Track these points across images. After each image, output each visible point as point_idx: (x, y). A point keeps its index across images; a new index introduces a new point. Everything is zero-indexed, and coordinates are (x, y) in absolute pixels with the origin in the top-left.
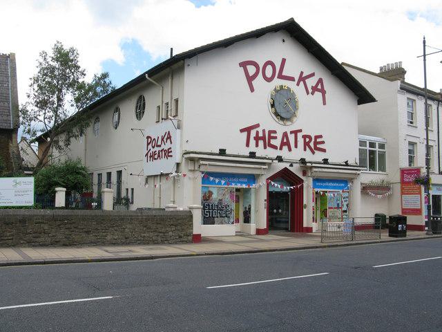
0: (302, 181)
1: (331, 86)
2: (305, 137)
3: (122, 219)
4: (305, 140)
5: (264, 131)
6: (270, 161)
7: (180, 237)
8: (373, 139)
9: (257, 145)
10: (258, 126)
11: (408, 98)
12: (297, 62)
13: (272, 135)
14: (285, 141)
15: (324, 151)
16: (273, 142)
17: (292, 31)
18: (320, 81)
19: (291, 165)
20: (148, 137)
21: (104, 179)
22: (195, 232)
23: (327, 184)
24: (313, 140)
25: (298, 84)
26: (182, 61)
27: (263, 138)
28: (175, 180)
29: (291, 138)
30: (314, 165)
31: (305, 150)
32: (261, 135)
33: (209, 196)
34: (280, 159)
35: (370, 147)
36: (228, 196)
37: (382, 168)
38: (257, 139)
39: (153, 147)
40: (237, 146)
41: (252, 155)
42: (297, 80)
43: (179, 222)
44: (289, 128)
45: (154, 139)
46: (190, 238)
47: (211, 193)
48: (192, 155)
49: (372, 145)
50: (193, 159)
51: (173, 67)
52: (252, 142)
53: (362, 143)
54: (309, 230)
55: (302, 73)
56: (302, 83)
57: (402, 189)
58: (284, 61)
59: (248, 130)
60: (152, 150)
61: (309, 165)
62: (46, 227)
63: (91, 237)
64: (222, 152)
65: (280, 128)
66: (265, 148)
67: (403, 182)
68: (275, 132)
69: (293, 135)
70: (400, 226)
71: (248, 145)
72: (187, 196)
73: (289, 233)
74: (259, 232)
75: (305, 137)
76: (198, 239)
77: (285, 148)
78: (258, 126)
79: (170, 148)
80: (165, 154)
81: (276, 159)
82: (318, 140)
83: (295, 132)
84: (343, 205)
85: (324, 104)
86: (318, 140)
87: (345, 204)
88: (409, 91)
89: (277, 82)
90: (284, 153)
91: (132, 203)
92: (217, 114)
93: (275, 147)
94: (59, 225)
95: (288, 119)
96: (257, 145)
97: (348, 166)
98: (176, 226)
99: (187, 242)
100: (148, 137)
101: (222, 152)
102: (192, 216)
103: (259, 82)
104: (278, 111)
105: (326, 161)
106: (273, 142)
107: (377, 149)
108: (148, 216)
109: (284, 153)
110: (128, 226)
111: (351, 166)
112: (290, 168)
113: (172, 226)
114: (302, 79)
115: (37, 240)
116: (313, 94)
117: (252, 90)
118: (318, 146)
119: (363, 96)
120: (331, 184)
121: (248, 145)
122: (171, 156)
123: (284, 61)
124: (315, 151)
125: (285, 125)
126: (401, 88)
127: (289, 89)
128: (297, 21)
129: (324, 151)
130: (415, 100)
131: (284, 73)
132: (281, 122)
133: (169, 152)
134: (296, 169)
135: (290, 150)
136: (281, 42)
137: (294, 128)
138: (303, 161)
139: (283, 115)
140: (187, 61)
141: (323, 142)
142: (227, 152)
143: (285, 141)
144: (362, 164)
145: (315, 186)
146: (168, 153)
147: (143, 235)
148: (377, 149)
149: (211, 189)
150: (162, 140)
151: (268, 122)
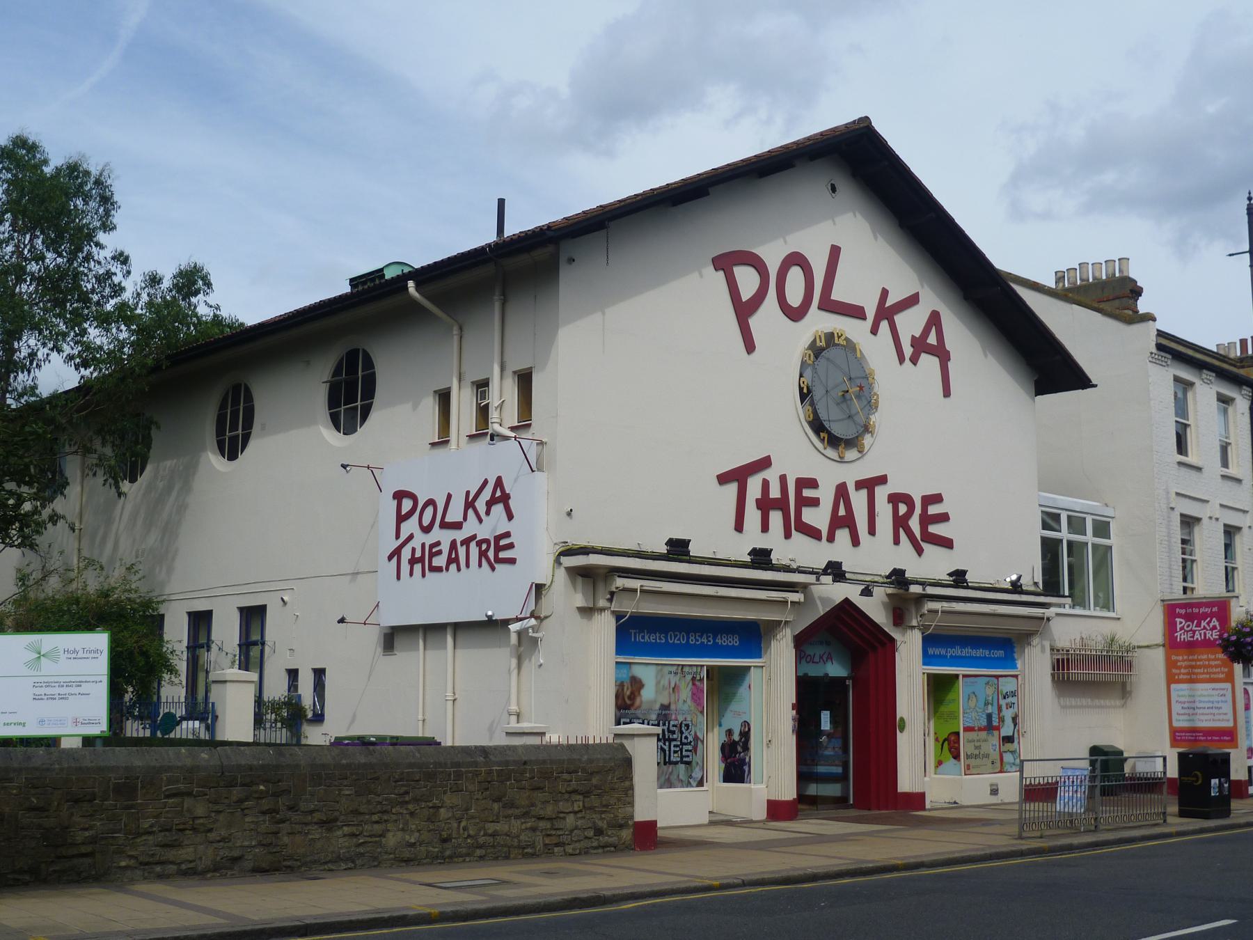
0: (892, 640)
1: (960, 335)
2: (895, 499)
3: (430, 776)
4: (895, 510)
5: (783, 479)
6: (811, 579)
7: (599, 832)
8: (1078, 503)
9: (765, 528)
10: (765, 463)
11: (1177, 379)
12: (873, 264)
13: (807, 493)
14: (842, 512)
15: (947, 543)
16: (809, 516)
17: (859, 160)
18: (935, 320)
19: (867, 592)
20: (399, 496)
21: (226, 631)
22: (641, 813)
23: (957, 651)
24: (918, 510)
25: (874, 330)
26: (550, 248)
27: (782, 504)
28: (528, 643)
29: (859, 500)
30: (931, 590)
31: (897, 541)
32: (775, 493)
33: (633, 696)
34: (835, 571)
35: (1096, 533)
36: (686, 692)
37: (1106, 602)
38: (765, 505)
39: (426, 530)
40: (718, 537)
41: (761, 558)
42: (871, 313)
43: (594, 781)
44: (851, 474)
45: (431, 502)
46: (626, 834)
47: (637, 684)
48: (594, 560)
49: (1076, 524)
50: (592, 574)
51: (516, 271)
52: (753, 515)
53: (1050, 520)
54: (917, 800)
55: (885, 293)
56: (884, 325)
57: (1170, 665)
58: (835, 252)
59: (738, 476)
60: (420, 538)
61: (915, 589)
62: (200, 810)
63: (340, 841)
64: (678, 549)
65: (830, 472)
66: (788, 535)
67: (1172, 644)
68: (813, 484)
69: (864, 492)
70: (1215, 782)
71: (739, 527)
72: (567, 693)
73: (853, 813)
74: (777, 810)
75: (895, 499)
76: (647, 836)
77: (843, 535)
78: (765, 463)
79: (507, 535)
80: (483, 554)
81: (825, 572)
82: (933, 510)
83: (869, 485)
84: (1002, 720)
85: (947, 393)
86: (933, 510)
87: (1008, 714)
88: (1179, 357)
89: (819, 322)
90: (840, 550)
91: (319, 718)
92: (654, 417)
93: (814, 533)
94: (241, 801)
95: (851, 443)
96: (765, 528)
97: (1023, 592)
98: (586, 794)
99: (617, 849)
100: (399, 496)
101: (678, 549)
102: (628, 762)
103: (767, 318)
104: (823, 415)
105: (959, 578)
106: (809, 516)
107: (1089, 538)
108: (507, 763)
109: (840, 550)
110: (449, 799)
111: (787, 569)
112: (862, 603)
113: (565, 794)
114: (886, 313)
115: (171, 854)
116: (914, 360)
117: (750, 347)
118: (933, 529)
119: (1050, 368)
120: (968, 652)
121: (739, 527)
122: (512, 561)
123: (835, 252)
124: (924, 545)
125: (841, 461)
126: (1160, 347)
127: (850, 346)
128: (878, 126)
129: (947, 543)
130: (1192, 384)
131: (836, 295)
132: (831, 453)
133: (498, 549)
134: (875, 609)
135: (856, 542)
136: (827, 192)
137: (867, 470)
138: (898, 577)
139: (838, 429)
140: (567, 249)
141: (944, 518)
142: (694, 550)
143: (842, 512)
144: (1051, 585)
145: (927, 659)
146: (497, 551)
147: (491, 828)
148: (1089, 538)
149: (638, 672)
150: (469, 504)
151: (798, 455)
